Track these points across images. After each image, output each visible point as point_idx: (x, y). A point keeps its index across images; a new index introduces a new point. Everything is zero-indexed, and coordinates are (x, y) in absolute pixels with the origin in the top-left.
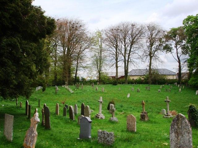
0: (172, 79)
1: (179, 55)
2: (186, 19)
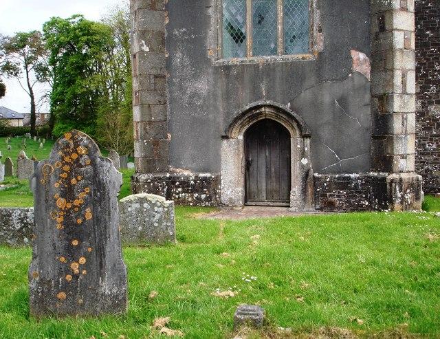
0: (17, 126)
1: (31, 84)
2: (49, 23)
